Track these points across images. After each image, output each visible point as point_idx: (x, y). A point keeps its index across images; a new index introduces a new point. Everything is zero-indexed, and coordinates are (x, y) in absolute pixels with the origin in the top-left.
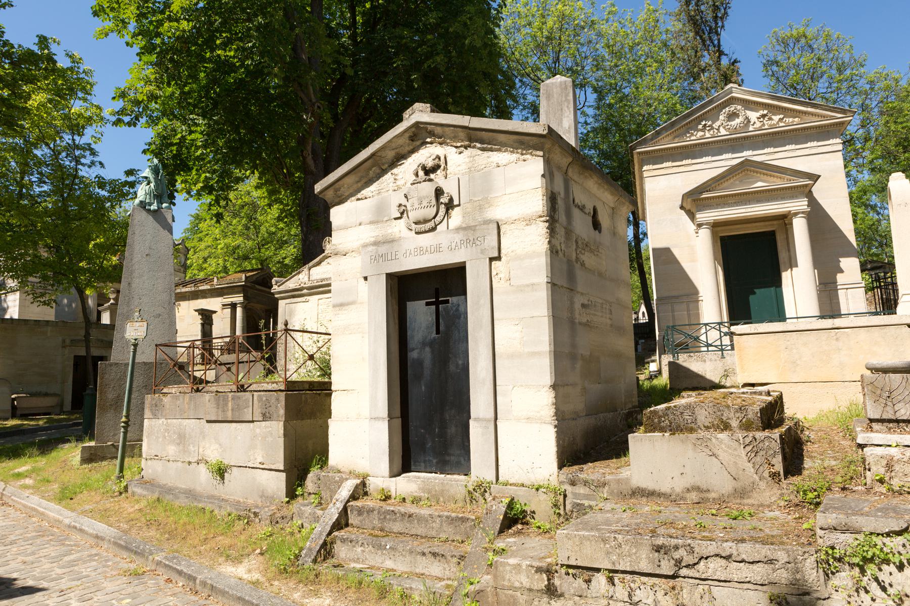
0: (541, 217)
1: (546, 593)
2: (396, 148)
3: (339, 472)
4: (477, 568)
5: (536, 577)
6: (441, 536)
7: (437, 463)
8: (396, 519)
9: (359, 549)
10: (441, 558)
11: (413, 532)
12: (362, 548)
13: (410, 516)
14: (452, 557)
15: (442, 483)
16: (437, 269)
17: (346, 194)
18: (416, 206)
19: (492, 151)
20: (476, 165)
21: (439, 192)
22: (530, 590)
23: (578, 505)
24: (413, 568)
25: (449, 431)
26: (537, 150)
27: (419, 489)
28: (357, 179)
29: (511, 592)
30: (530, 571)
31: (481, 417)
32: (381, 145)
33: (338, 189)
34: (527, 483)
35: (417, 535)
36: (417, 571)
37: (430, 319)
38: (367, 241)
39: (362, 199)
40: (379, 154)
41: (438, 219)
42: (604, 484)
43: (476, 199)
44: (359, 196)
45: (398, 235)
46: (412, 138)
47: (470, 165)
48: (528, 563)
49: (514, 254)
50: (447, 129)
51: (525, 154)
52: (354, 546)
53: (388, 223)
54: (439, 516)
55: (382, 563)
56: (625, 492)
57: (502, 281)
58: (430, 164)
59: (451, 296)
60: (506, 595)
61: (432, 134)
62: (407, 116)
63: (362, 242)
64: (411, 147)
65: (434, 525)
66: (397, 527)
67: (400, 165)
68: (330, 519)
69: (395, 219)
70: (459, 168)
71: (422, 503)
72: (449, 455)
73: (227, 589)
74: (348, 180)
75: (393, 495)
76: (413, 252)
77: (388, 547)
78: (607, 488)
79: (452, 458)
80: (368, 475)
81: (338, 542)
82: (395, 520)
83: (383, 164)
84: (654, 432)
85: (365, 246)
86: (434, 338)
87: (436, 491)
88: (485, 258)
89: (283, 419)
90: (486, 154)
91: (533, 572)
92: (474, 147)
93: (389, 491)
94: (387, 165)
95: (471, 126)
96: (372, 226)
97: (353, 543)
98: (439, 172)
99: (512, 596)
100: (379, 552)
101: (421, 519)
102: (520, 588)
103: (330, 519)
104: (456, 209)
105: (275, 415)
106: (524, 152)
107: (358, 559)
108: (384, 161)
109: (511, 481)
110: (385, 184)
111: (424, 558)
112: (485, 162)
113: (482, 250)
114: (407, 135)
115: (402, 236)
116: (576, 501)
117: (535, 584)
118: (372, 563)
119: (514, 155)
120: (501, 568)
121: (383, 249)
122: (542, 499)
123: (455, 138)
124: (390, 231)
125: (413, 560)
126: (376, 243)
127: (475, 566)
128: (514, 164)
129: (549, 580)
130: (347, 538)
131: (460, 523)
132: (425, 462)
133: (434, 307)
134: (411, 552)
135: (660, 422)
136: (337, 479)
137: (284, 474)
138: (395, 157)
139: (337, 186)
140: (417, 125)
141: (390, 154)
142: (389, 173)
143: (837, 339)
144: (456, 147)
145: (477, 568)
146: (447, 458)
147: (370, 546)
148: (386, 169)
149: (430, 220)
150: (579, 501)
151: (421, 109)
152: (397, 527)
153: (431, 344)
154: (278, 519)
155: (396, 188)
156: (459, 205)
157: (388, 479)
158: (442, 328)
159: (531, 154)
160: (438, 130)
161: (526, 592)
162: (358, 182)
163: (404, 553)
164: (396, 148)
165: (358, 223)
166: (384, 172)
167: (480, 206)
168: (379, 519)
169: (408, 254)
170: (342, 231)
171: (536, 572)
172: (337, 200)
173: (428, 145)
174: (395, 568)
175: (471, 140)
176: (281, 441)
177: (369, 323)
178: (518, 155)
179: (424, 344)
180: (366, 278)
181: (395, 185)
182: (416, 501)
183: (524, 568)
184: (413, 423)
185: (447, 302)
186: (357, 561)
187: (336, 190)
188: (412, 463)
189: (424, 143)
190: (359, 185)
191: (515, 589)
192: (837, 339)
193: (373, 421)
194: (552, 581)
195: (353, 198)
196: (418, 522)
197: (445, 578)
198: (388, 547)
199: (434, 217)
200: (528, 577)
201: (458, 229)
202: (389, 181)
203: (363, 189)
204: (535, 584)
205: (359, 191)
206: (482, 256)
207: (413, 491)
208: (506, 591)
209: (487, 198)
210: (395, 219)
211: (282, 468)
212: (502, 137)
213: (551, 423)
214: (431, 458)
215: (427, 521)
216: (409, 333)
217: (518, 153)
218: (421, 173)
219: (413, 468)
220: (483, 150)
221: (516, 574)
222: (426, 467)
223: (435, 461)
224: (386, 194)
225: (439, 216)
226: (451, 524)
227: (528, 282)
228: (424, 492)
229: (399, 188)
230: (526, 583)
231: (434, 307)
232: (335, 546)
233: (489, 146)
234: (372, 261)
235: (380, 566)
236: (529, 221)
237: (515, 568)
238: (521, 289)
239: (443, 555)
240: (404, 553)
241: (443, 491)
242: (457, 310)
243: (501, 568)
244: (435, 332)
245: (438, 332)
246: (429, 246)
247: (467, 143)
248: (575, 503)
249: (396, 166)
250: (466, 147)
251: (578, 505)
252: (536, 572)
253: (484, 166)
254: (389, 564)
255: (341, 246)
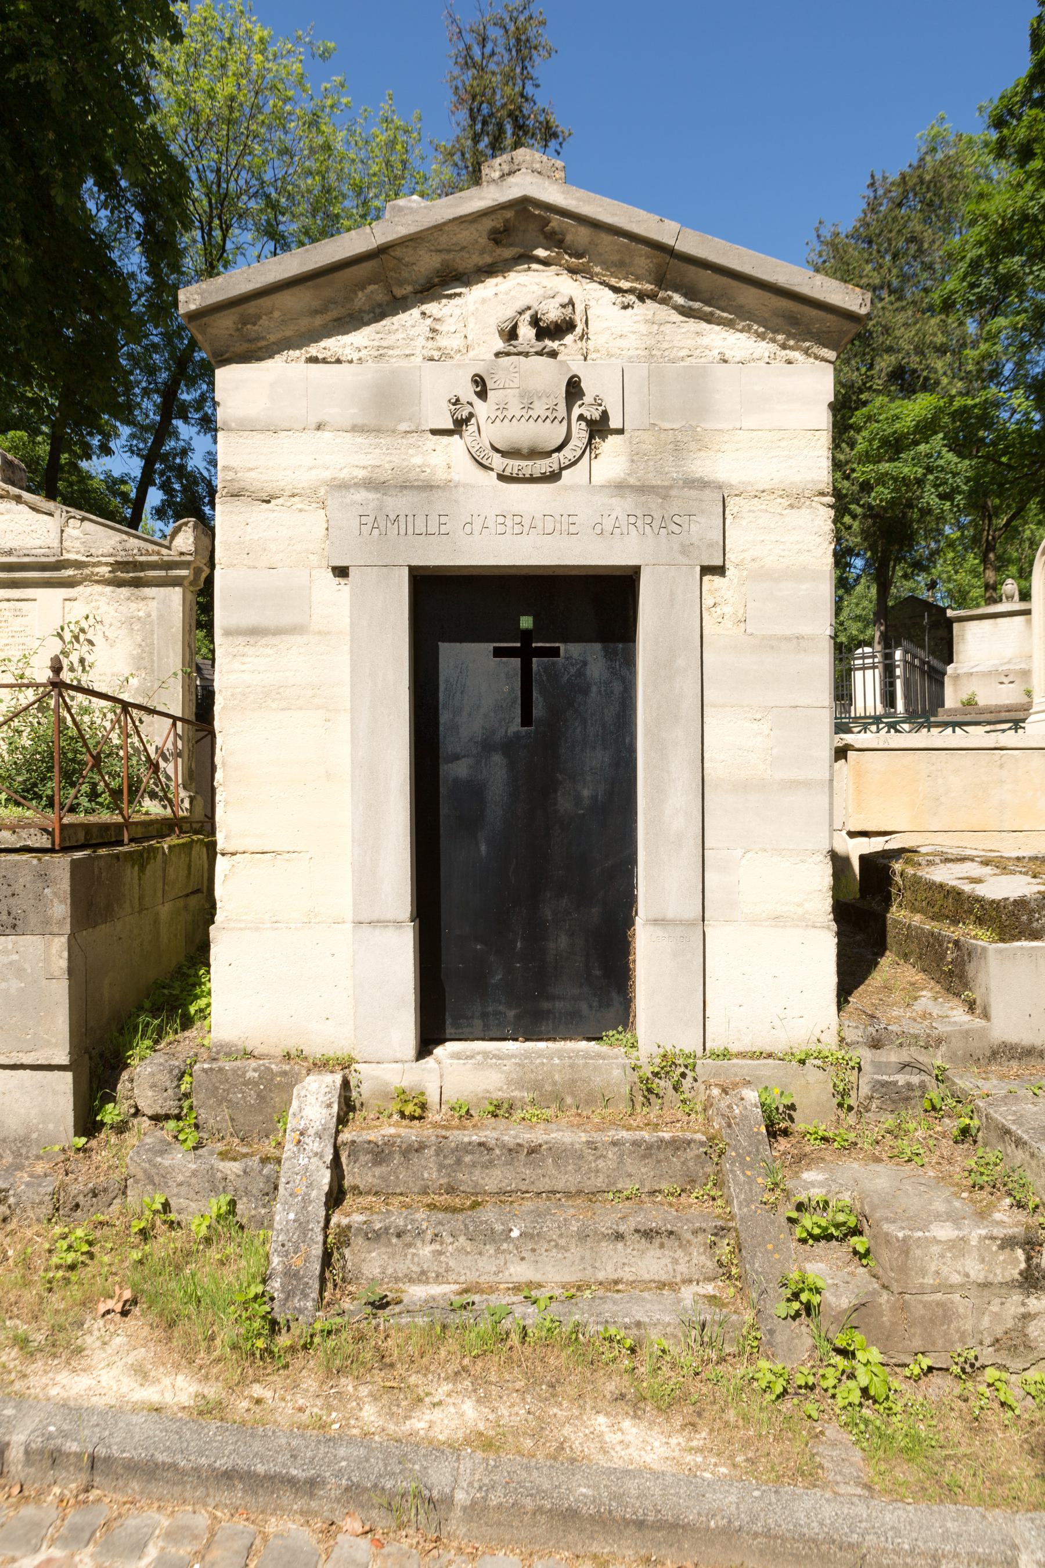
0: (822, 494)
1: (1020, 1287)
2: (449, 251)
3: (249, 1055)
4: (776, 1249)
5: (1001, 1258)
6: (620, 1186)
7: (518, 1018)
8: (491, 1161)
9: (426, 1251)
10: (665, 1240)
11: (544, 1184)
12: (437, 1247)
13: (533, 1151)
14: (695, 1232)
15: (571, 1066)
16: (561, 573)
17: (272, 338)
18: (515, 409)
19: (709, 322)
20: (665, 345)
21: (574, 390)
22: (986, 1285)
23: (883, 1086)
24: (590, 1270)
25: (551, 945)
26: (825, 346)
27: (509, 1083)
28: (316, 304)
29: (938, 1296)
30: (989, 1246)
31: (670, 914)
32: (413, 229)
33: (254, 320)
34: (778, 1048)
35: (554, 1192)
36: (601, 1276)
37: (506, 689)
38: (344, 475)
39: (324, 361)
40: (398, 252)
41: (568, 455)
42: (939, 1041)
43: (667, 426)
44: (313, 350)
45: (441, 475)
46: (498, 237)
47: (651, 342)
48: (983, 1232)
49: (755, 565)
50: (606, 238)
51: (791, 348)
52: (409, 1245)
53: (413, 439)
54: (614, 1144)
55: (496, 1274)
56: (979, 1053)
57: (728, 623)
58: (552, 314)
59: (565, 640)
60: (926, 1305)
61: (555, 240)
62: (496, 175)
63: (327, 475)
64: (488, 259)
65: (601, 1164)
66: (493, 1180)
67: (450, 297)
68: (310, 1186)
69: (435, 432)
70: (620, 343)
71: (518, 1114)
72: (552, 998)
73: (161, 1458)
74: (287, 300)
75: (433, 1098)
76: (490, 523)
77: (515, 1233)
78: (943, 1048)
79: (559, 1005)
80: (352, 1060)
81: (358, 1242)
82: (490, 1164)
83: (401, 283)
84: (1019, 939)
85: (342, 486)
86: (517, 735)
87: (555, 1084)
88: (692, 566)
89: (67, 928)
90: (694, 325)
91: (994, 1248)
92: (664, 301)
93: (422, 1094)
94: (409, 289)
95: (682, 246)
96: (360, 439)
97: (408, 1238)
98: (569, 339)
99: (939, 1304)
100: (490, 1249)
101: (560, 1154)
102: (962, 1285)
103: (310, 1186)
104: (612, 439)
105: (33, 919)
106: (792, 343)
107: (423, 1273)
108: (405, 275)
109: (734, 1049)
110: (400, 335)
111: (620, 1245)
112: (689, 343)
113: (682, 545)
114: (488, 224)
115: (456, 478)
116: (879, 1077)
117: (998, 1271)
118: (471, 1277)
119: (764, 344)
120: (918, 1252)
121: (398, 504)
122: (811, 1079)
123: (621, 267)
124: (417, 460)
125: (588, 1254)
126: (370, 484)
127: (770, 1247)
128: (762, 364)
129: (1029, 1259)
130: (387, 1229)
131: (669, 1152)
132: (484, 1016)
133: (516, 662)
134: (583, 1237)
135: (1030, 921)
136: (251, 1074)
137: (68, 1076)
138: (438, 273)
139: (251, 308)
140: (523, 205)
141: (427, 262)
142: (415, 312)
143: (1001, 766)
144: (616, 290)
145: (776, 1249)
146: (546, 1005)
147: (462, 1239)
148: (404, 298)
149: (549, 454)
150: (885, 1078)
151: (537, 166)
152: (493, 1180)
153: (509, 747)
154: (81, 1199)
155: (436, 355)
156: (620, 432)
157: (415, 1065)
158: (538, 710)
159: (806, 352)
160: (581, 235)
161: (974, 1292)
162: (316, 312)
163: (562, 1242)
164: (449, 251)
165: (313, 421)
166: (396, 305)
167: (676, 442)
168: (441, 1167)
169: (477, 527)
170: (258, 436)
171: (1002, 1247)
172: (240, 348)
173: (534, 266)
174: (537, 1278)
175: (663, 280)
176: (60, 992)
177: (353, 686)
178: (773, 347)
179: (487, 746)
180: (341, 572)
181: (430, 344)
182: (501, 1110)
183: (973, 1243)
184: (452, 927)
185: (555, 652)
186: (422, 1277)
187: (245, 321)
188: (448, 1022)
189: (526, 258)
190: (318, 321)
191: (951, 1288)
192: (1001, 766)
193: (365, 930)
194: (1035, 1261)
195: (294, 354)
196: (555, 1162)
197: (678, 1280)
198: (515, 1233)
199: (559, 449)
200: (983, 1261)
201: (620, 487)
202: (413, 332)
203: (329, 336)
204: (998, 1271)
205: (315, 336)
206: (684, 560)
207: (491, 1088)
208: (926, 1298)
209: (693, 429)
210: (435, 432)
211: (64, 1059)
212: (750, 296)
213: (828, 928)
214: (501, 1008)
215: (581, 1157)
216: (444, 718)
217: (773, 341)
218: (525, 332)
219: (450, 1031)
220: (686, 312)
221: (954, 1258)
222: (486, 1027)
223: (511, 1014)
224: (404, 363)
225: (570, 446)
226: (644, 1157)
227: (788, 632)
228: (522, 1088)
229: (445, 355)
230: (976, 1270)
231: (516, 662)
232: (347, 1252)
233: (708, 309)
234: (365, 529)
235: (492, 1278)
236: (795, 499)
237: (953, 1247)
238: (770, 644)
239: (671, 1233)
240: (562, 1242)
241: (574, 1081)
242: (580, 674)
243: (918, 1252)
244: (519, 720)
245: (527, 719)
246: (539, 516)
247: (649, 287)
248: (878, 1081)
249: (437, 298)
250: (642, 297)
251: (884, 1084)
252: (1002, 1247)
253: (684, 353)
254: (520, 1271)
255: (252, 475)
